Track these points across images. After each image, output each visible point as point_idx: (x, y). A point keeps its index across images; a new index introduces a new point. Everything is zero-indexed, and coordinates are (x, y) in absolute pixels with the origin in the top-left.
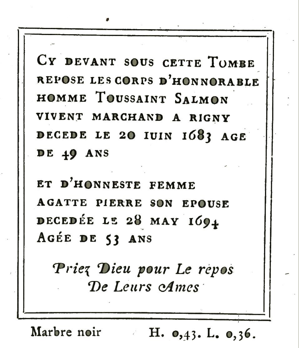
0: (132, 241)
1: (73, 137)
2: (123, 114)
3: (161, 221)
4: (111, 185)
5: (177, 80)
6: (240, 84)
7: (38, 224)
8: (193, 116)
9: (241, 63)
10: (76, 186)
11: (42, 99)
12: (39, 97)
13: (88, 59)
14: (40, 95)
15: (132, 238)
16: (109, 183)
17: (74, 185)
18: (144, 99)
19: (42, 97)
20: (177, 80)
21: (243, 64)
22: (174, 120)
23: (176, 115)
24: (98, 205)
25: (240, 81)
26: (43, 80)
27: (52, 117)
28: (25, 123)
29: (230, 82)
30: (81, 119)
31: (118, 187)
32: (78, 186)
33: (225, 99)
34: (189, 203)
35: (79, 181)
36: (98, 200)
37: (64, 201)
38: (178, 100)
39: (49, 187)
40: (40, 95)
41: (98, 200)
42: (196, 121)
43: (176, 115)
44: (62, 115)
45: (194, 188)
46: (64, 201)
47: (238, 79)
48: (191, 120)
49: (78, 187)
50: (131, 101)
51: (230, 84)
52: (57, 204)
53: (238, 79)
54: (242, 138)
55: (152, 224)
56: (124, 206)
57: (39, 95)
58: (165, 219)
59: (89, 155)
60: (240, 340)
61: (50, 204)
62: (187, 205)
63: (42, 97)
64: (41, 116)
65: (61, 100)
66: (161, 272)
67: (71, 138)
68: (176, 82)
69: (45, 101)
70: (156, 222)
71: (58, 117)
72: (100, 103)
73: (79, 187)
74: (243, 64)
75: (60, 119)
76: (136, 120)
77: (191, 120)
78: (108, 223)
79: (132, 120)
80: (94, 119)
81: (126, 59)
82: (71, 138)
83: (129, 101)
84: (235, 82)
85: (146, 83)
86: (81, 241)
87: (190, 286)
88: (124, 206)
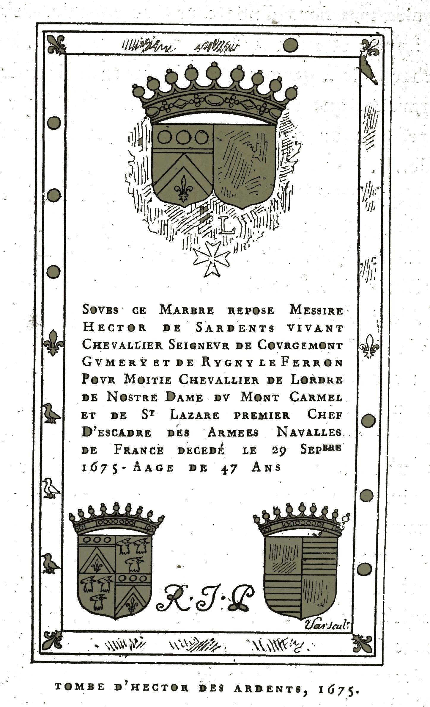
1: (86, 435)
2: (114, 430)
4: (206, 346)
6: (194, 312)
7: (268, 383)
9: (192, 311)
11: (136, 688)
12: (85, 324)
13: (293, 325)
14: (192, 378)
16: (203, 344)
17: (139, 686)
18: (151, 381)
19: (194, 379)
21: (109, 310)
22: (252, 361)
24: (236, 418)
25: (110, 309)
27: (299, 433)
29: (219, 380)
30: (121, 331)
31: (309, 313)
33: (280, 688)
34: (244, 311)
37: (265, 364)
38: (85, 311)
39: (291, 692)
40: (192, 378)
42: (334, 314)
45: (218, 418)
48: (230, 313)
50: (318, 313)
55: (107, 365)
56: (188, 313)
59: (209, 330)
60: (264, 232)
61: (193, 347)
63: (194, 379)
65: (296, 313)
67: (210, 453)
69: (205, 366)
70: (233, 435)
71: (199, 468)
72: (130, 342)
73: (136, 690)
74: (109, 310)
75: (99, 436)
76: (326, 314)
77: (230, 313)
80: (292, 313)
81: (278, 470)
82: (210, 453)
83: (316, 313)
84: (243, 688)
85: (251, 313)
86: (268, 383)
87: (161, 605)
88: (188, 313)
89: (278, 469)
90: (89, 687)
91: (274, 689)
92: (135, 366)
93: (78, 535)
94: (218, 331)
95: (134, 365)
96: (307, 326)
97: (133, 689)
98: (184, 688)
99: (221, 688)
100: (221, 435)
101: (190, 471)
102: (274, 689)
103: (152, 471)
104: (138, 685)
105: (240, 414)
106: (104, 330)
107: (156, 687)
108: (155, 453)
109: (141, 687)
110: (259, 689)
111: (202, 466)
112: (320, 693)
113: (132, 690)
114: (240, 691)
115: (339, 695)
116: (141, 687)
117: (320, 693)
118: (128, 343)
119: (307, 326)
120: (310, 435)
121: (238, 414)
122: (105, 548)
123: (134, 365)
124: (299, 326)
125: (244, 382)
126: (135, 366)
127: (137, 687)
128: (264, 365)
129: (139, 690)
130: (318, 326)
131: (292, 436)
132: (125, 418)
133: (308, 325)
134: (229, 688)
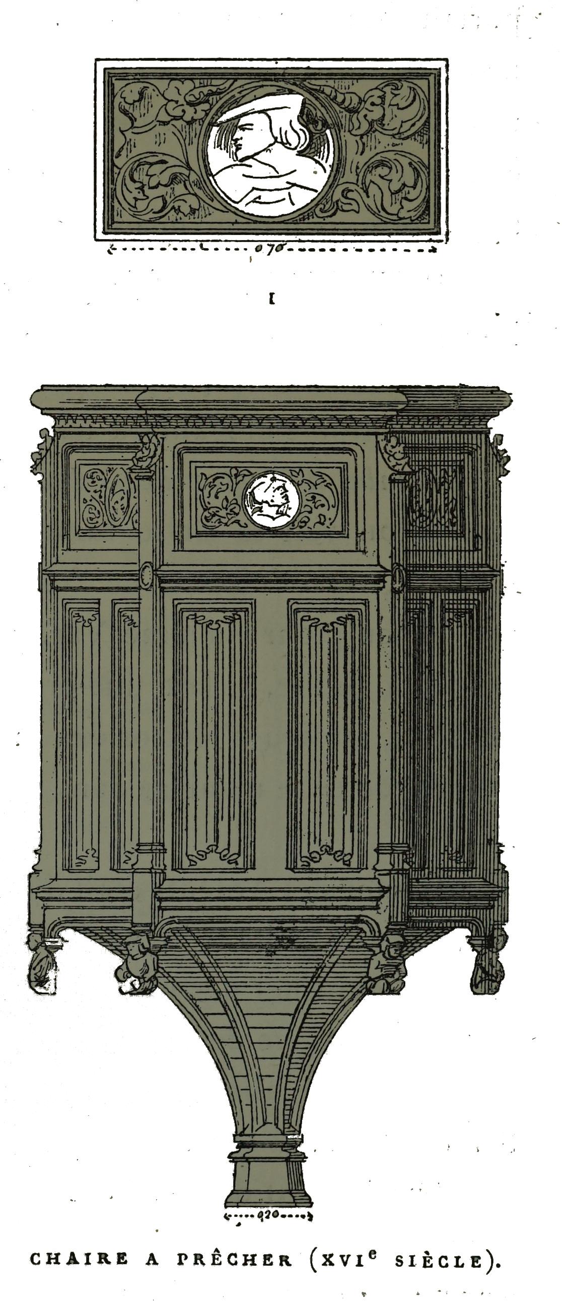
0: (72, 1261)
2: (34, 1255)
3: (64, 1258)
5: (250, 1258)
8: (284, 1258)
10: (57, 1255)
11: (54, 1261)
12: (245, 1259)
13: (349, 1256)
15: (72, 1258)
18: (81, 1258)
20: (250, 1258)
22: (148, 1264)
23: (152, 1255)
24: (180, 1263)
26: (202, 1259)
28: (93, 128)
29: (151, 1258)
32: (53, 1261)
35: (251, 1255)
36: (180, 1255)
37: (463, 1264)
41: (180, 1255)
43: (152, 1255)
44: (198, 1258)
46: (463, 1264)
47: (100, 1254)
49: (236, 1259)
51: (151, 1262)
52: (69, 1261)
53: (100, 1254)
54: (268, 1262)
57: (49, 1254)
58: (345, 1264)
62: (219, 1262)
64: (347, 1260)
66: (288, 183)
68: (249, 1260)
78: (462, 1266)
79: (236, 1259)
84: (112, 1258)
89: (399, 1264)
90: (100, 1258)
91: (276, 1260)
92: (290, 1265)
93: (304, 1189)
94: (100, 1262)
95: (288, 1264)
96: (342, 1257)
97: (57, 1255)
98: (284, 1260)
99: (399, 1261)
100: (284, 1263)
101: (455, 1266)
102: (276, 1260)
103: (157, 1264)
104: (49, 1262)
105: (186, 1258)
106: (220, 1264)
107: (444, 1262)
108: (39, 1263)
109: (259, 1260)
110: (103, 1258)
111: (473, 1258)
112: (361, 1256)
113: (47, 1263)
114: (76, 1262)
115: (295, 171)
116: (259, 1260)
117: (361, 1256)
118: (86, 1254)
119: (342, 1257)
120: (74, 1263)
121: (183, 1257)
122: (390, 618)
123: (288, 1264)
124: (88, 1263)
125: (415, 1259)
126: (290, 1265)
127: (253, 1260)
128: (462, 1266)
129: (59, 1263)
130: (72, 1254)
131: (327, 1265)
132: (126, 1262)
133: (344, 1256)
134: (299, 1260)
